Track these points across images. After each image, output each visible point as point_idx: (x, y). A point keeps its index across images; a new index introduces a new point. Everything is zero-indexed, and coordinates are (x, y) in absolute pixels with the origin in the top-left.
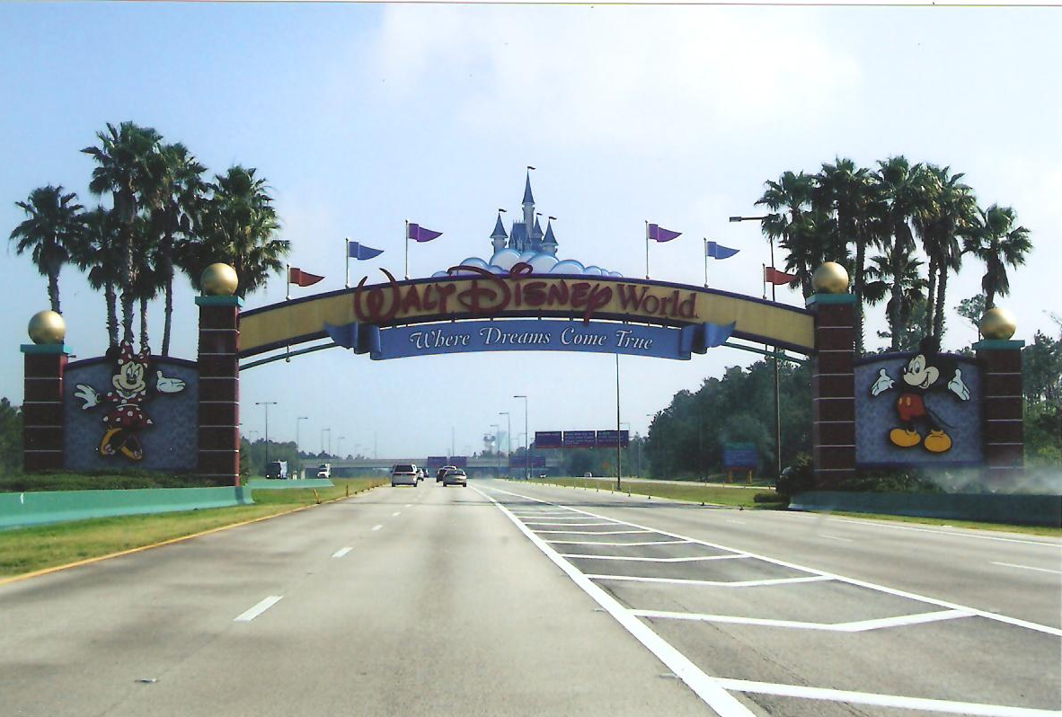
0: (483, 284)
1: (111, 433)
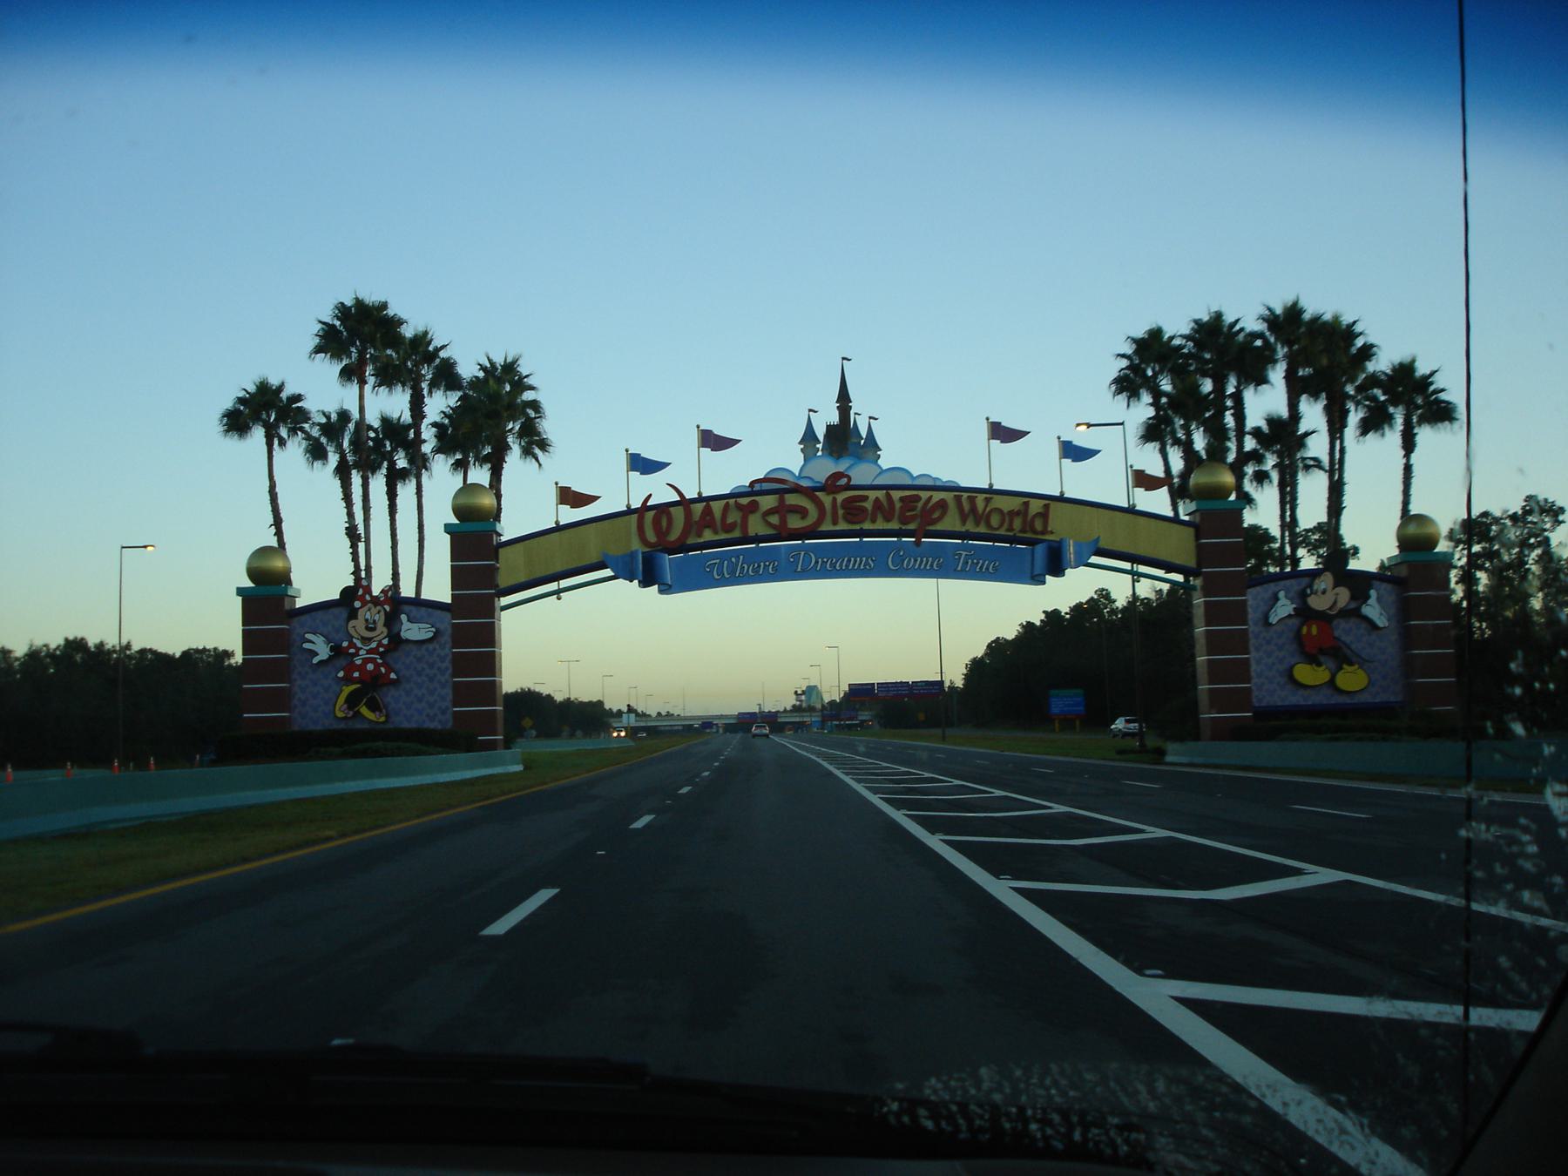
0: (792, 499)
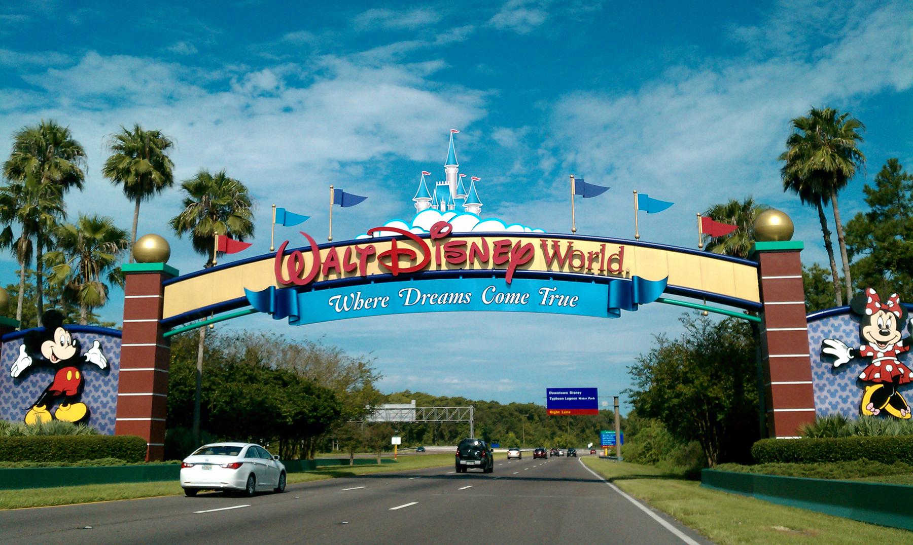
0: (401, 245)
1: (871, 390)
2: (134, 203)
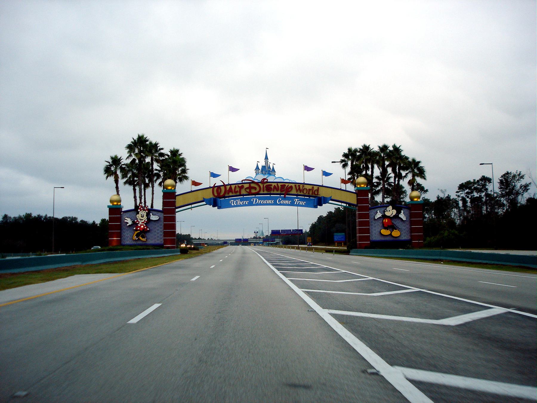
0: (252, 185)
1: (136, 233)
2: (106, 175)
